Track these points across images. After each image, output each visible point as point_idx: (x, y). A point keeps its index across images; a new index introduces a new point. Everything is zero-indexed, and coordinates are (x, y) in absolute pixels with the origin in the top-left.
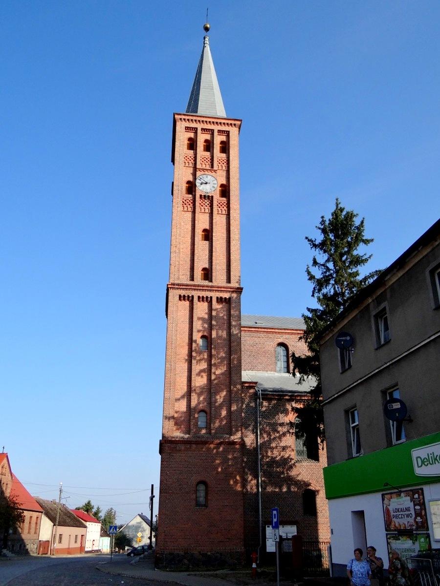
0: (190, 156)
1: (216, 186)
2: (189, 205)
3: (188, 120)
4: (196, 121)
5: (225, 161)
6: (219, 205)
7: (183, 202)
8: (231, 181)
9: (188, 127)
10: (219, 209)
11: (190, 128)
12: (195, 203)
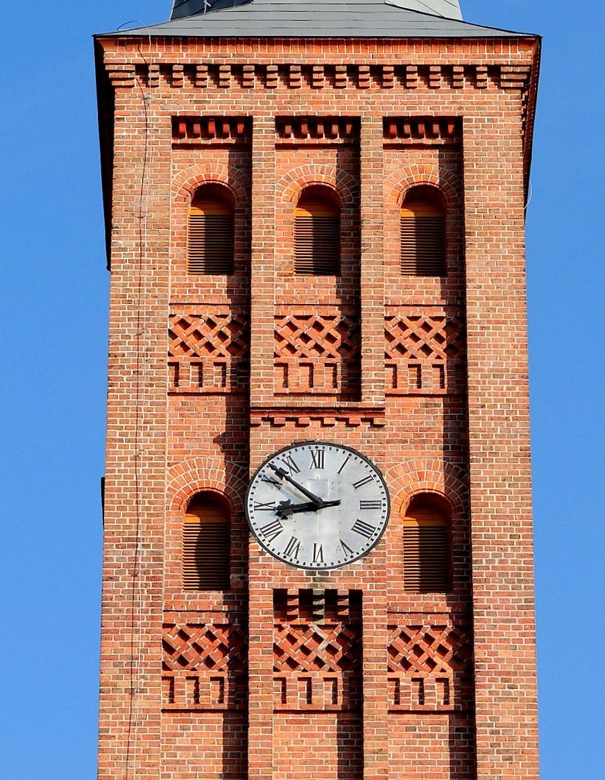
0: (208, 313)
1: (375, 518)
2: (209, 663)
3: (190, 70)
4: (424, 71)
5: (438, 327)
6: (406, 651)
7: (168, 648)
8: (479, 472)
9: (190, 121)
10: (404, 676)
11: (204, 121)
12: (244, 649)
